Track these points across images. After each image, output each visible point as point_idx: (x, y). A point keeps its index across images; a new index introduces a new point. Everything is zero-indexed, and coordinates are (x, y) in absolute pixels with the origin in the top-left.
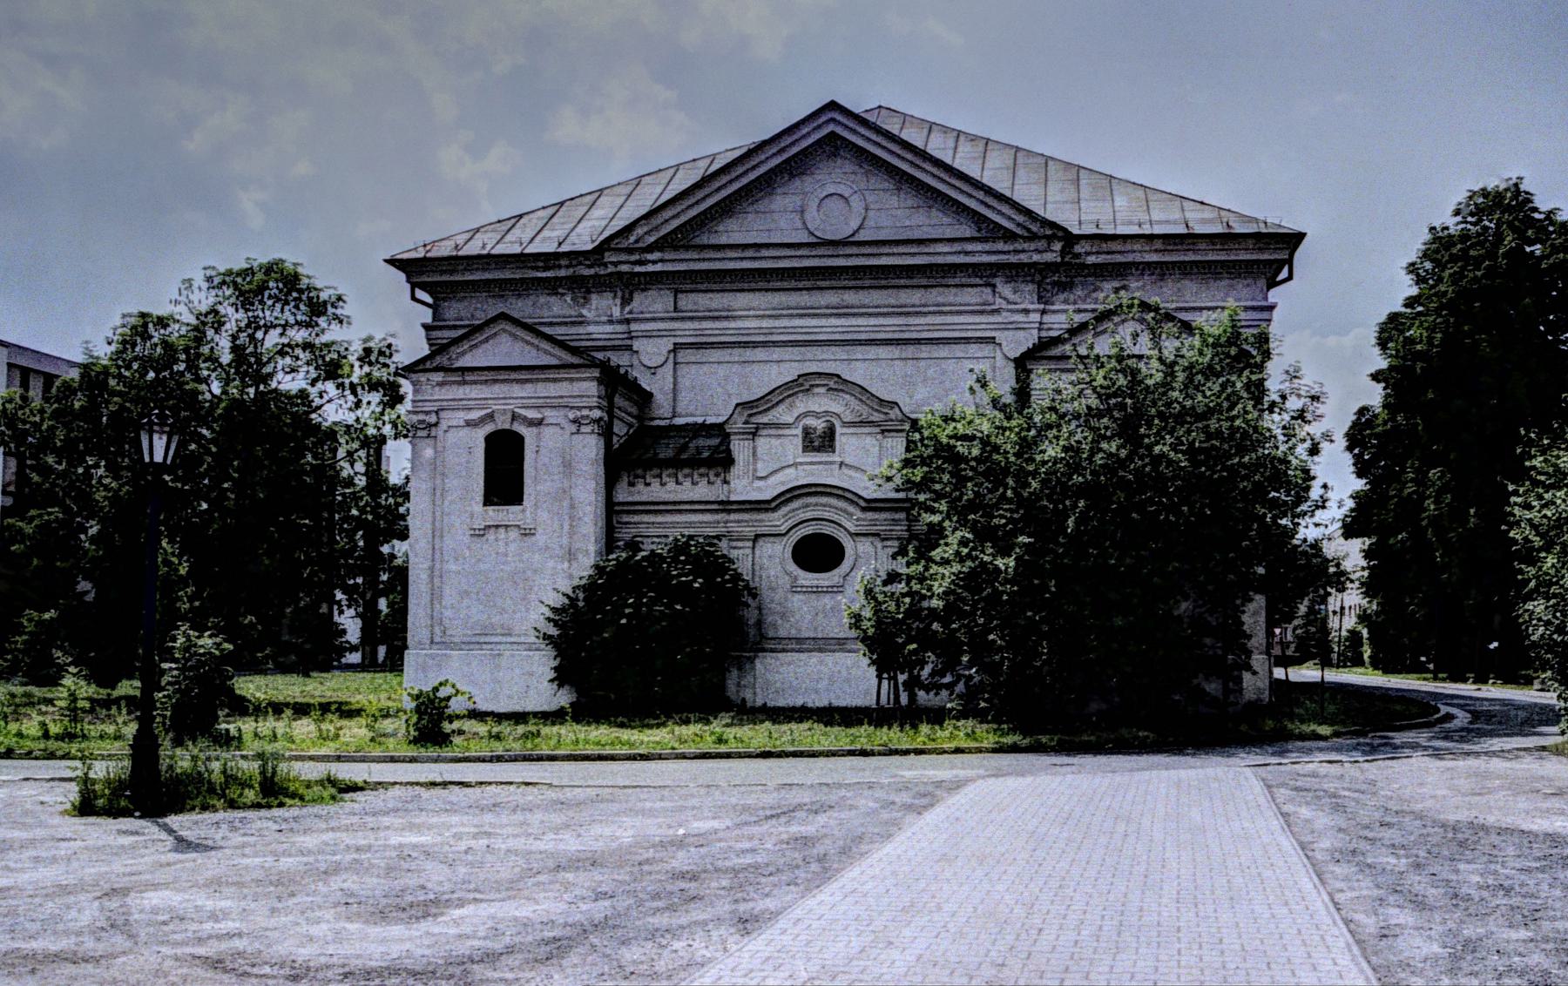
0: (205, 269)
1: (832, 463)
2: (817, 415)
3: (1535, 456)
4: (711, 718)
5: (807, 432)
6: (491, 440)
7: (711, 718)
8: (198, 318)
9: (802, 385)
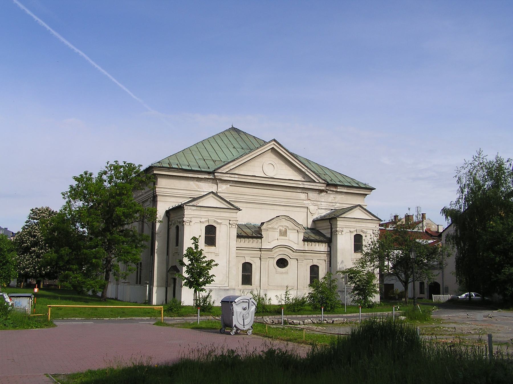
0: (237, 247)
1: (287, 239)
2: (282, 226)
3: (499, 258)
4: (35, 21)
5: (280, 231)
6: (207, 227)
7: (35, 21)
8: (497, 352)
9: (280, 218)
